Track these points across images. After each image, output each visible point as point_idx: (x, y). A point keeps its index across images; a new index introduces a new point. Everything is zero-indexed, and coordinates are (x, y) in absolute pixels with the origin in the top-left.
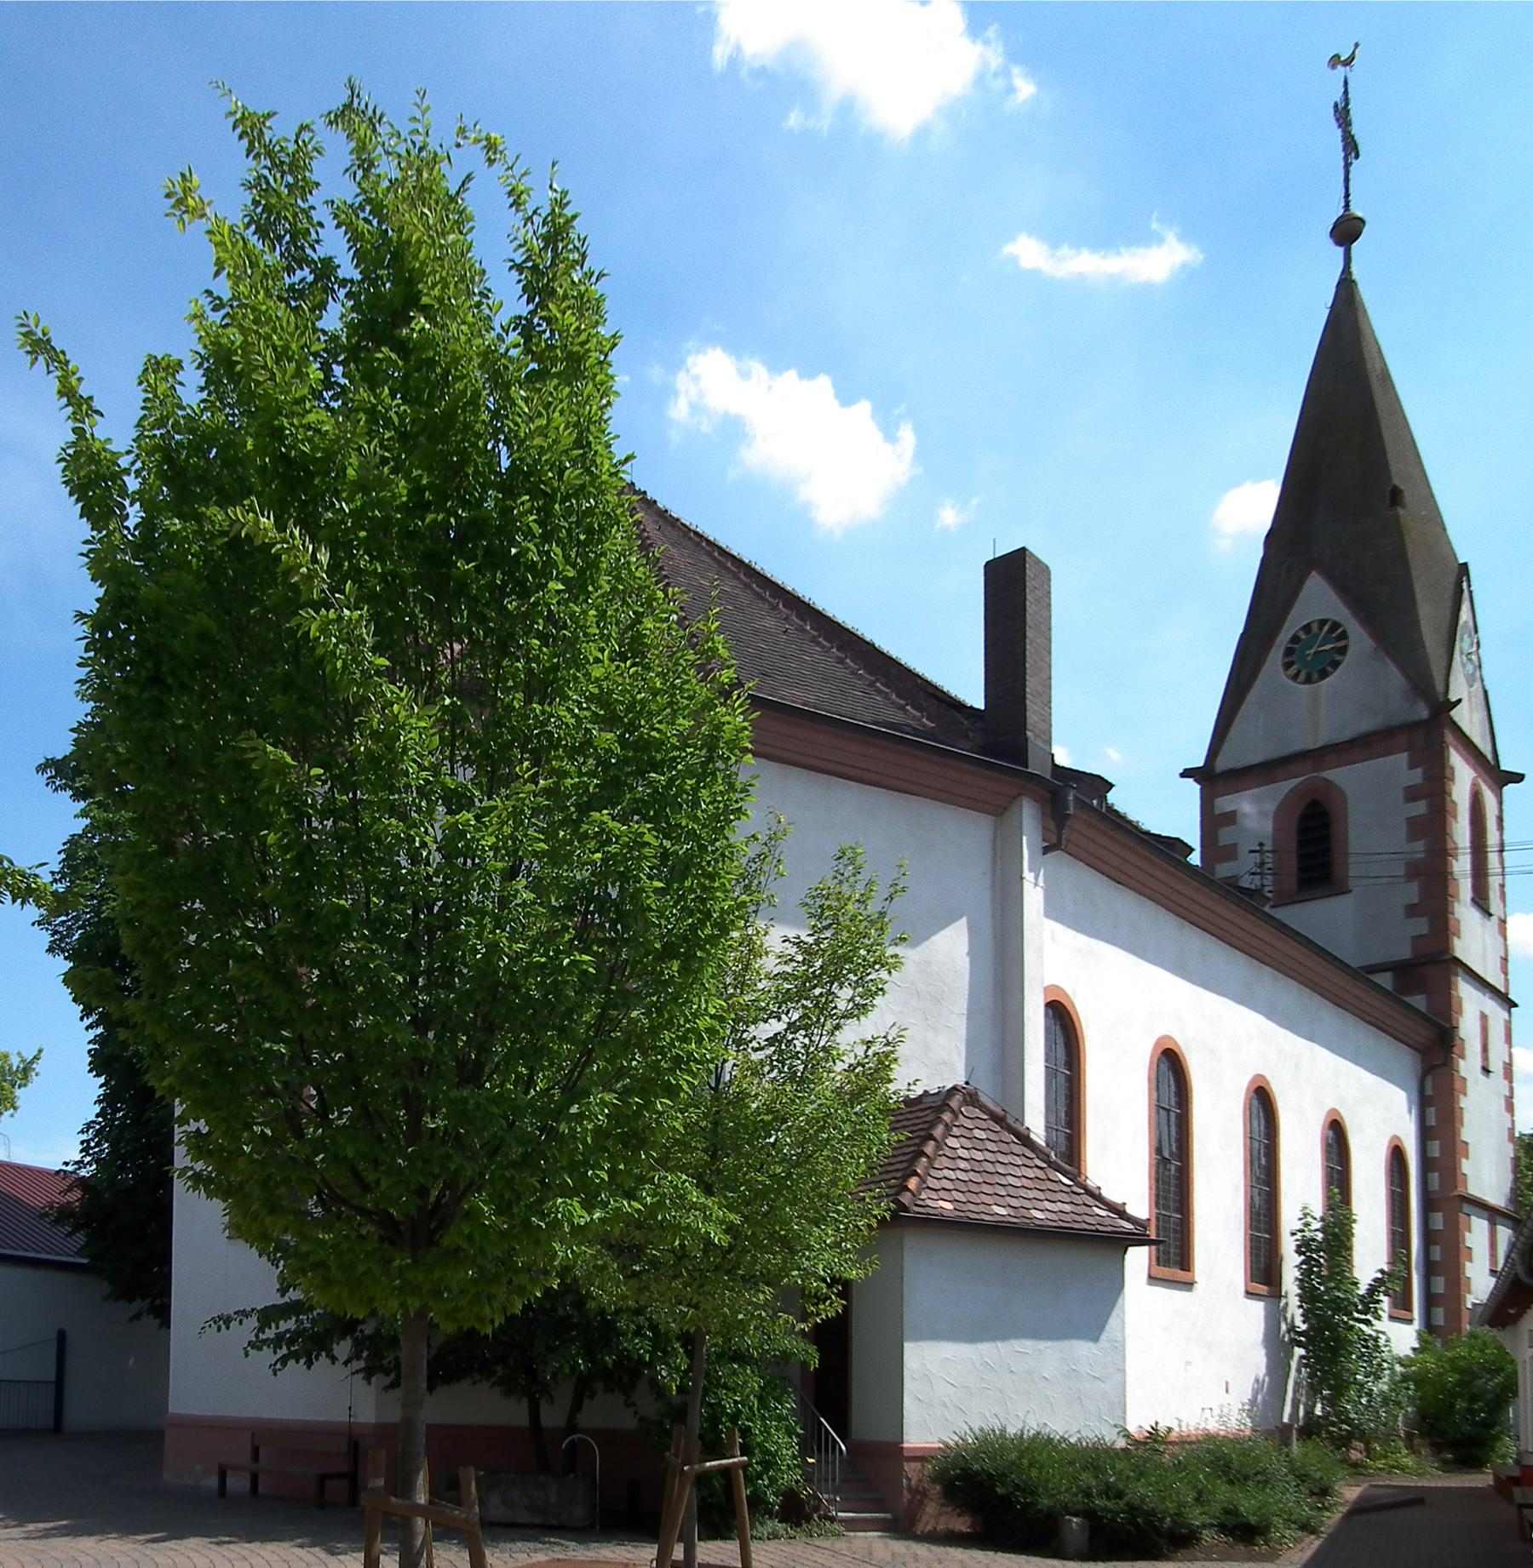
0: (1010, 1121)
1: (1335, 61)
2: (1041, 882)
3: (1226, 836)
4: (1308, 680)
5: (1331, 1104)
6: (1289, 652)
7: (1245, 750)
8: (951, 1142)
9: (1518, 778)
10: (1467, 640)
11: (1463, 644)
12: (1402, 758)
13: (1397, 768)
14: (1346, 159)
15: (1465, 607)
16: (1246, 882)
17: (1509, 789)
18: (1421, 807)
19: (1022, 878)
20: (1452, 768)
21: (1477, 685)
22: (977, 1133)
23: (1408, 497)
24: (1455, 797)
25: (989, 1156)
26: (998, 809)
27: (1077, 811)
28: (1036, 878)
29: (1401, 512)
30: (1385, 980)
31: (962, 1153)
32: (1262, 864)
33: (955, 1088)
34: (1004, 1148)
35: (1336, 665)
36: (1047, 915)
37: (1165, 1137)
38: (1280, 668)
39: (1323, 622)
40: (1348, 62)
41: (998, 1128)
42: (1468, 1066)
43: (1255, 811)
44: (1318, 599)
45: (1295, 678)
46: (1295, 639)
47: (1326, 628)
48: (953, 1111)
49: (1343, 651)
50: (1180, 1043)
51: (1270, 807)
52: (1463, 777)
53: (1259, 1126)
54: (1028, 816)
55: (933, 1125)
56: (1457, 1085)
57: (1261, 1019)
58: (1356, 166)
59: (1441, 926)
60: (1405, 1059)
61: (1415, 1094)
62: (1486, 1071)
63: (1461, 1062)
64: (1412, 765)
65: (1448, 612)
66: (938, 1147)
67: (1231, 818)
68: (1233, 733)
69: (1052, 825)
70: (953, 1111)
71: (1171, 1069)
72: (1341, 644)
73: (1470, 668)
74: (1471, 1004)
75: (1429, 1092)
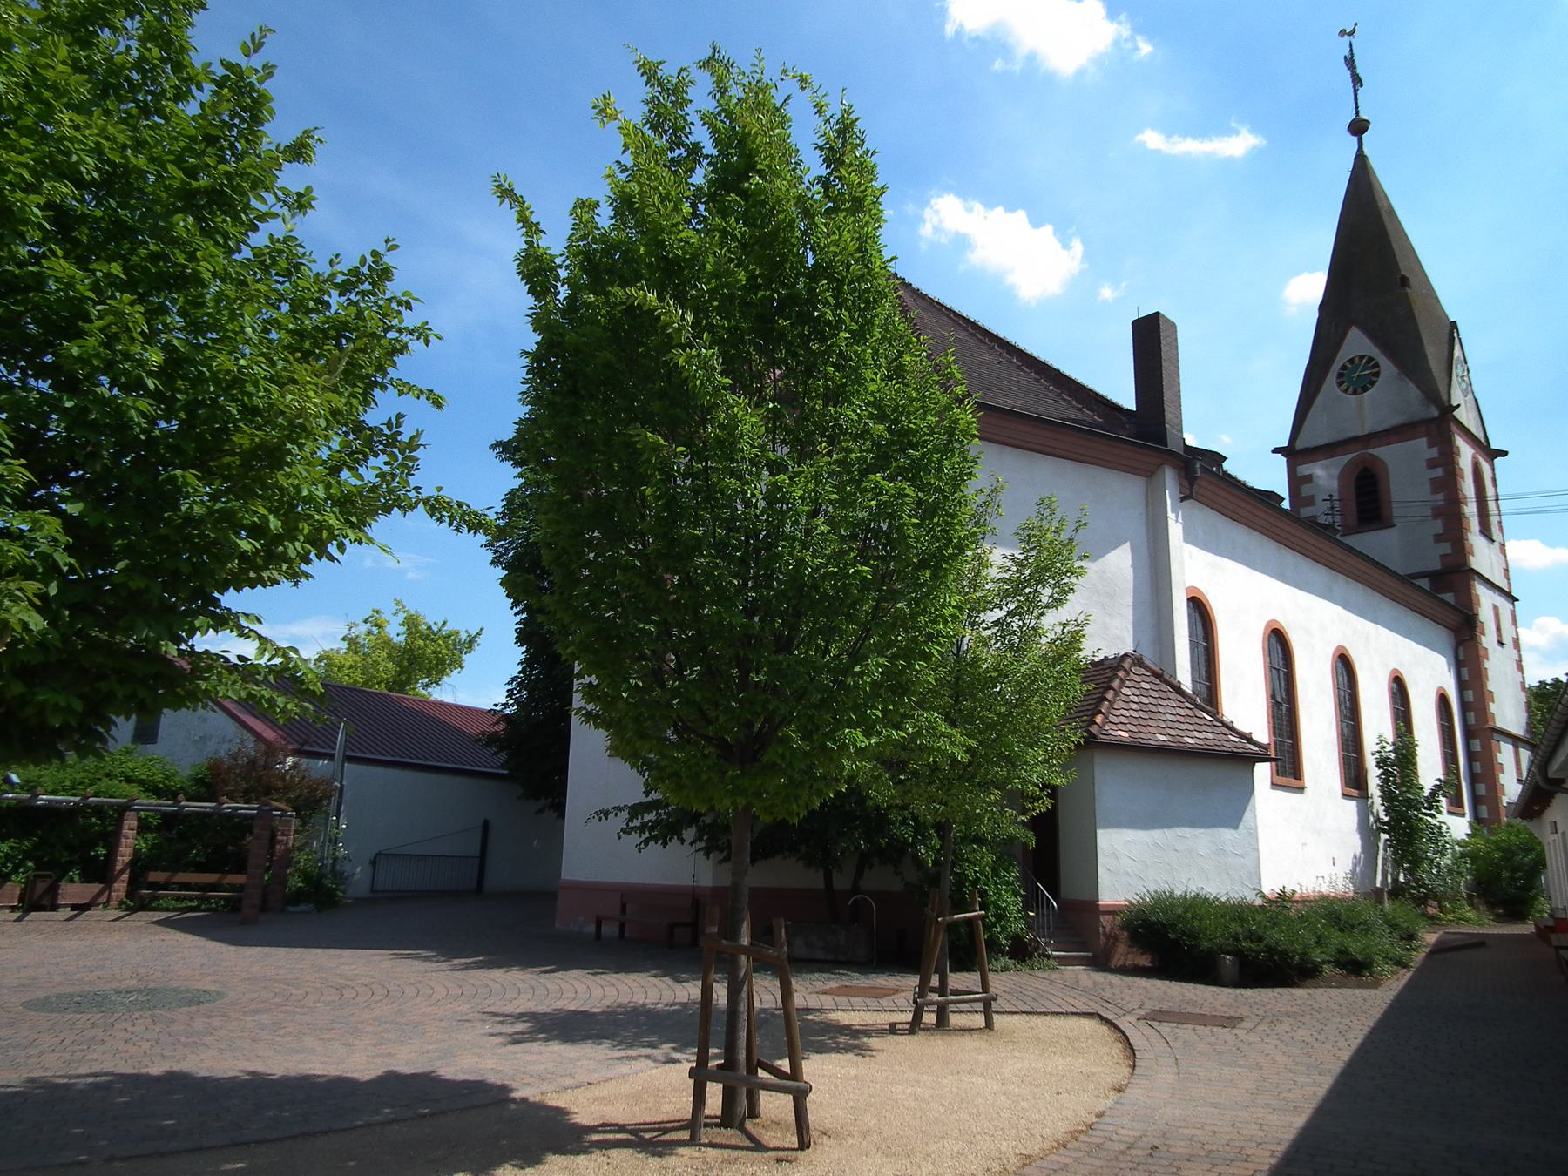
1: (1343, 33)
3: (1306, 490)
4: (1355, 393)
6: (1340, 375)
7: (1316, 434)
8: (1125, 691)
11: (1458, 370)
13: (1421, 447)
17: (1498, 461)
18: (1438, 472)
23: (1412, 281)
26: (1149, 473)
27: (1204, 476)
30: (1424, 583)
35: (1372, 383)
39: (1362, 357)
40: (1352, 33)
42: (1488, 640)
43: (1325, 475)
44: (1356, 343)
45: (1346, 391)
46: (1344, 367)
49: (1377, 374)
51: (1336, 472)
52: (1466, 455)
53: (1344, 680)
54: (1169, 477)
55: (1112, 679)
57: (1339, 609)
60: (1443, 636)
62: (1501, 643)
64: (1431, 445)
66: (1116, 694)
67: (1308, 479)
69: (1186, 484)
74: (1486, 601)
75: (1462, 657)
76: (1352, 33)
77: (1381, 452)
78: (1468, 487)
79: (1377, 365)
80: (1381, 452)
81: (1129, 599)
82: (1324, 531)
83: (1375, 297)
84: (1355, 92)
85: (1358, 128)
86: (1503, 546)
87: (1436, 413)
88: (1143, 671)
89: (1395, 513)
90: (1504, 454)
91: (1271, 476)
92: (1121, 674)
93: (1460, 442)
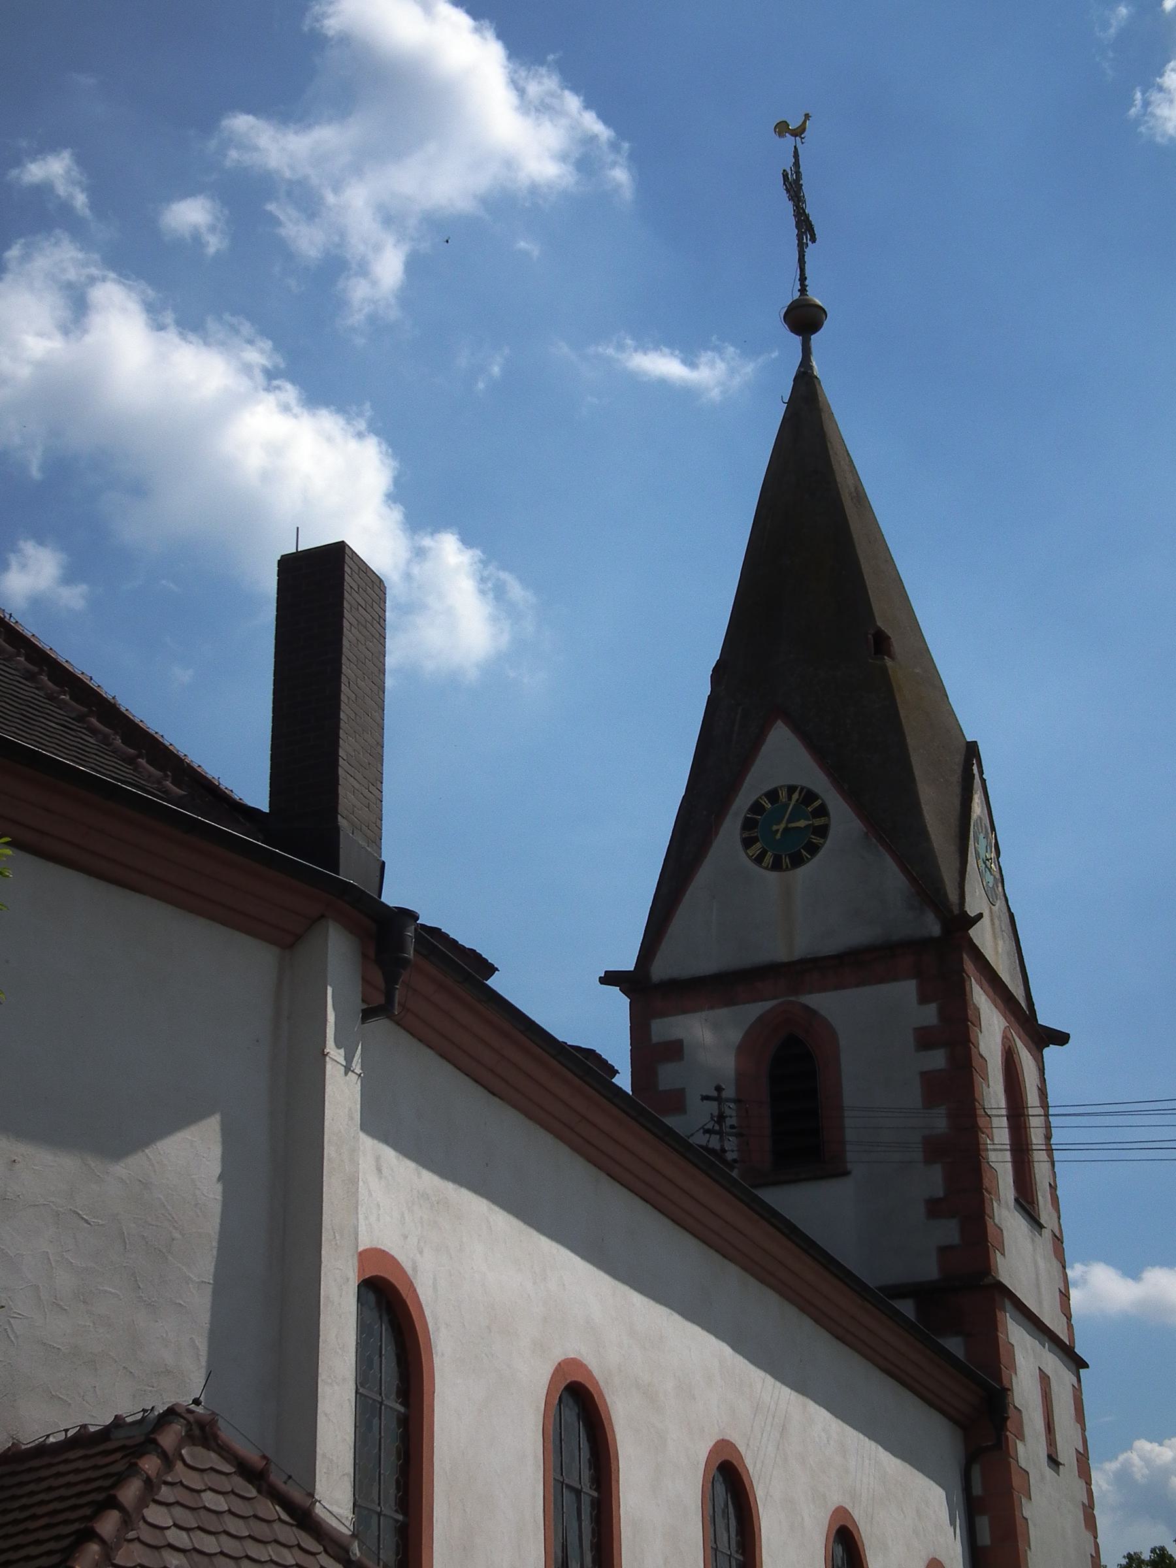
0: (276, 1479)
1: (782, 128)
2: (357, 1066)
3: (668, 1076)
4: (777, 866)
5: (836, 1499)
6: (748, 824)
7: (695, 952)
8: (155, 1514)
9: (1061, 1038)
10: (983, 842)
11: (978, 846)
12: (908, 989)
13: (902, 999)
14: (800, 238)
15: (977, 798)
16: (700, 1139)
17: (1051, 1053)
18: (937, 1060)
19: (325, 1055)
20: (977, 1010)
21: (1000, 903)
22: (209, 1499)
23: (897, 646)
24: (983, 1049)
25: (230, 1546)
26: (289, 938)
27: (430, 986)
28: (349, 1058)
29: (889, 662)
30: (907, 1308)
31: (174, 1536)
32: (721, 1118)
33: (172, 1412)
34: (260, 1530)
35: (813, 849)
36: (366, 1127)
37: (573, 1539)
38: (739, 845)
39: (791, 789)
40: (799, 132)
41: (252, 1492)
42: (1029, 1451)
43: (712, 1040)
44: (783, 760)
45: (759, 860)
46: (757, 808)
47: (795, 796)
48: (164, 1456)
49: (823, 831)
50: (596, 1373)
51: (735, 1036)
52: (991, 1029)
53: (728, 1539)
54: (337, 953)
55: (120, 1479)
56: (1016, 1481)
57: (727, 1350)
58: (810, 250)
59: (978, 1240)
60: (939, 1434)
61: (958, 1496)
62: (1054, 1461)
63: (1020, 1445)
64: (923, 999)
65: (957, 802)
66: (127, 1522)
67: (674, 1050)
68: (676, 927)
69: (379, 979)
70: (164, 1456)
71: (579, 1415)
72: (818, 822)
73: (989, 879)
74: (1027, 1361)
75: (977, 1490)
76: (799, 132)
77: (828, 1004)
78: (993, 1095)
79: (822, 811)
80: (828, 1004)
81: (205, 1267)
82: (707, 1162)
83: (816, 655)
84: (797, 164)
85: (804, 319)
86: (1058, 1240)
87: (936, 930)
88: (212, 1459)
89: (850, 1135)
90: (1061, 1038)
91: (600, 1025)
92: (150, 1464)
93: (981, 998)
